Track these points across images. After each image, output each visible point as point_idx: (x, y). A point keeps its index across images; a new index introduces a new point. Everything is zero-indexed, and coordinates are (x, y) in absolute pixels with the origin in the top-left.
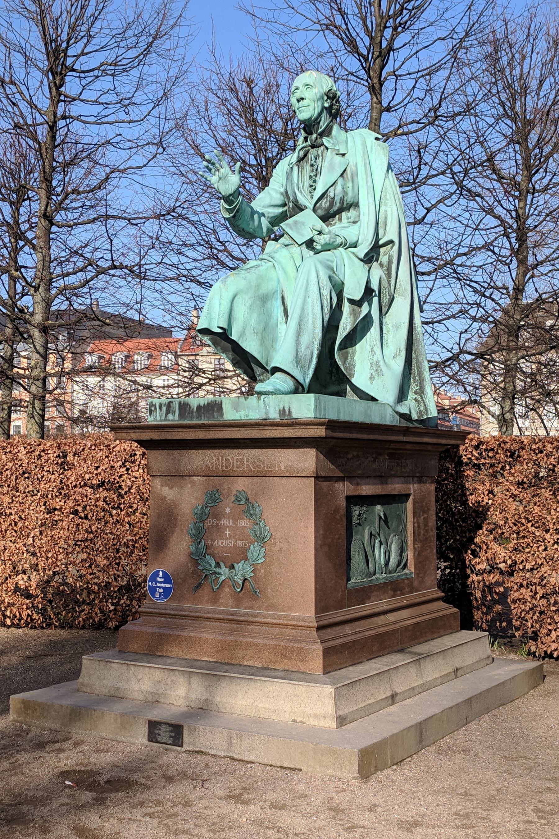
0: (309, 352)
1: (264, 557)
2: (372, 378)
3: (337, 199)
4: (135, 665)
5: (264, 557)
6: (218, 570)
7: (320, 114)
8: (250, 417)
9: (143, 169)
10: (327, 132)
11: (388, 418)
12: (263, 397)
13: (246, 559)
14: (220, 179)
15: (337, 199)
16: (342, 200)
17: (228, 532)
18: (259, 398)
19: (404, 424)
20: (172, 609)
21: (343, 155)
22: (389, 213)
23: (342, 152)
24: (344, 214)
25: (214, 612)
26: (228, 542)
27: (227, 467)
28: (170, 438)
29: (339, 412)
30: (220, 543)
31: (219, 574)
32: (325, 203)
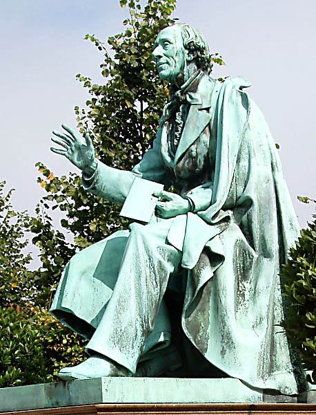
0: (132, 330)
2: (223, 352)
7: (182, 68)
10: (194, 87)
11: (244, 396)
19: (271, 401)
29: (146, 394)
32: (188, 163)
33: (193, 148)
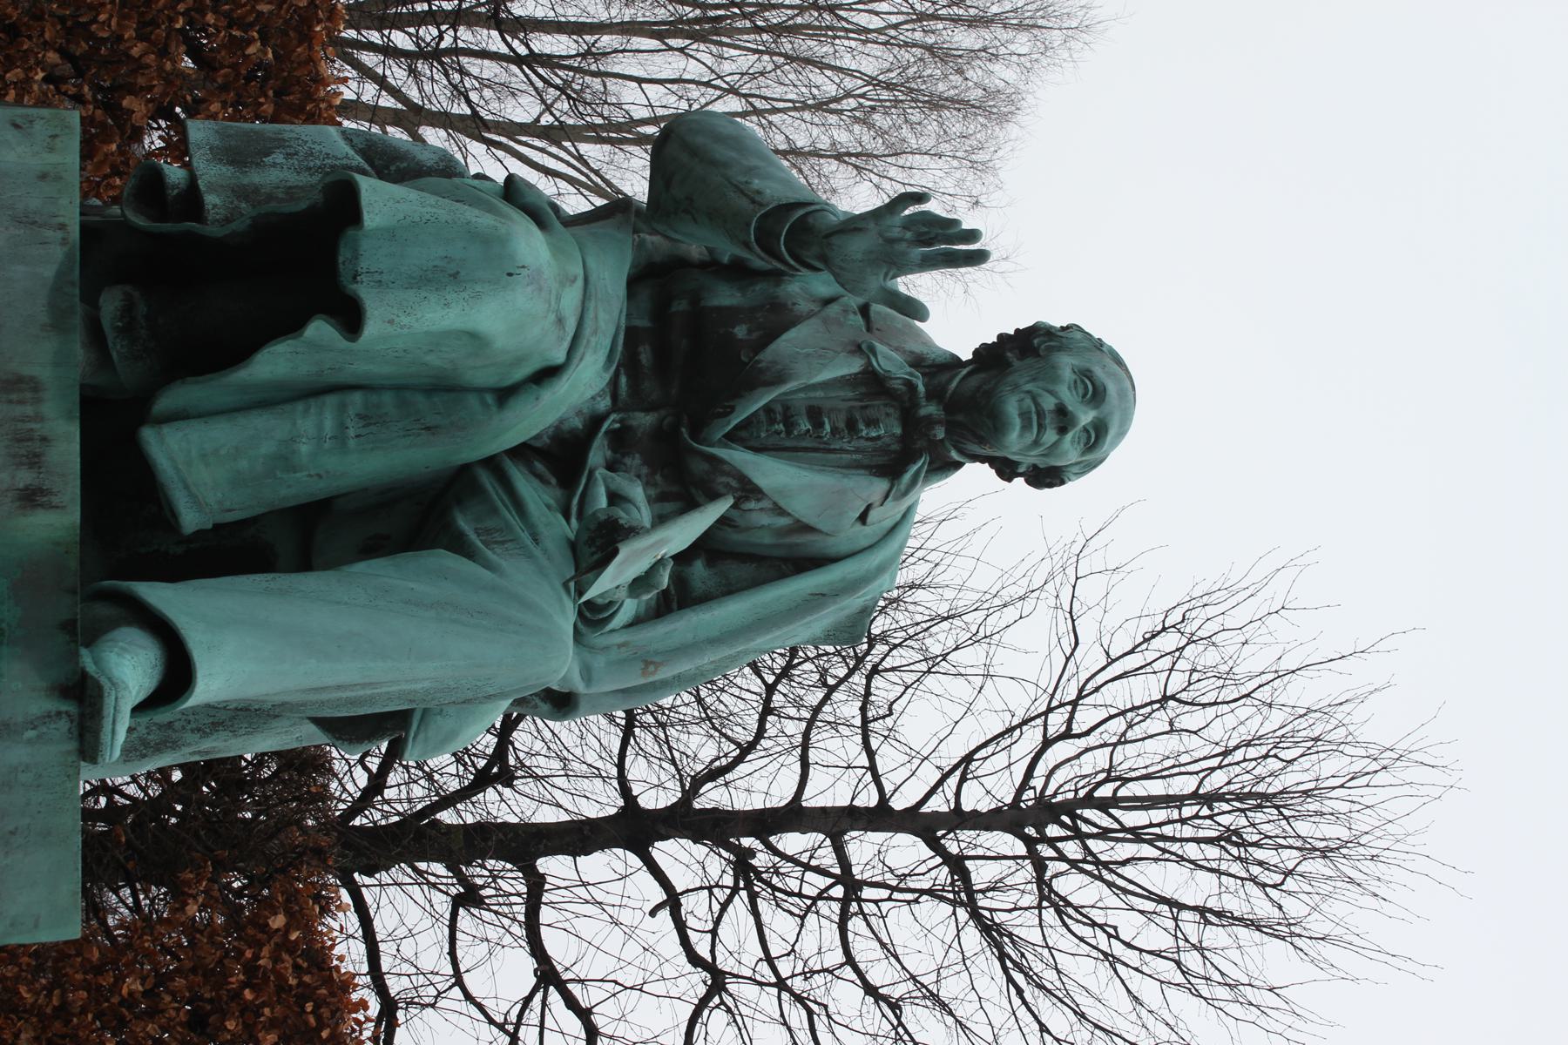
33: (765, 504)
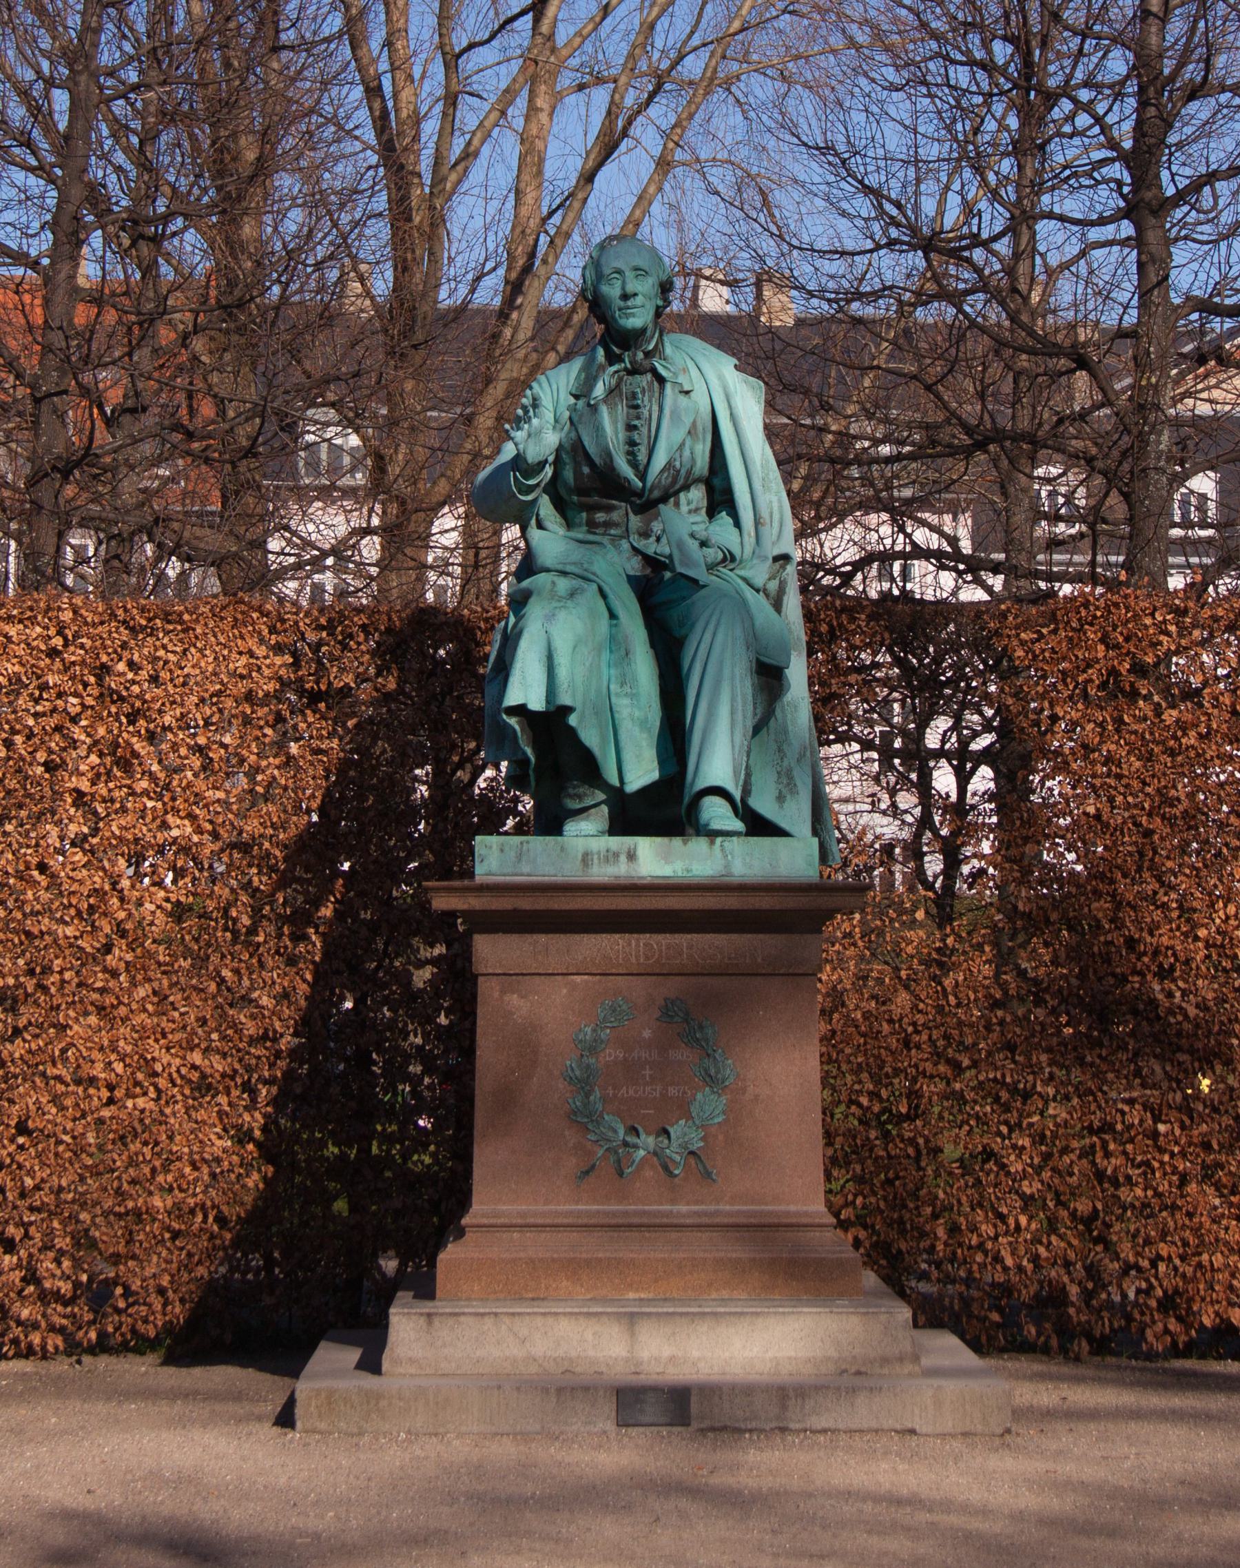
1: (724, 1112)
3: (683, 472)
4: (513, 1314)
5: (724, 1112)
6: (631, 1139)
8: (695, 872)
9: (765, 514)
12: (719, 840)
13: (689, 1117)
14: (529, 435)
15: (683, 472)
16: (689, 472)
17: (648, 1072)
18: (712, 843)
20: (483, 1216)
21: (687, 393)
22: (775, 505)
23: (686, 388)
24: (682, 495)
25: (626, 1213)
26: (648, 1089)
27: (647, 958)
28: (556, 907)
30: (631, 1092)
31: (636, 1147)
